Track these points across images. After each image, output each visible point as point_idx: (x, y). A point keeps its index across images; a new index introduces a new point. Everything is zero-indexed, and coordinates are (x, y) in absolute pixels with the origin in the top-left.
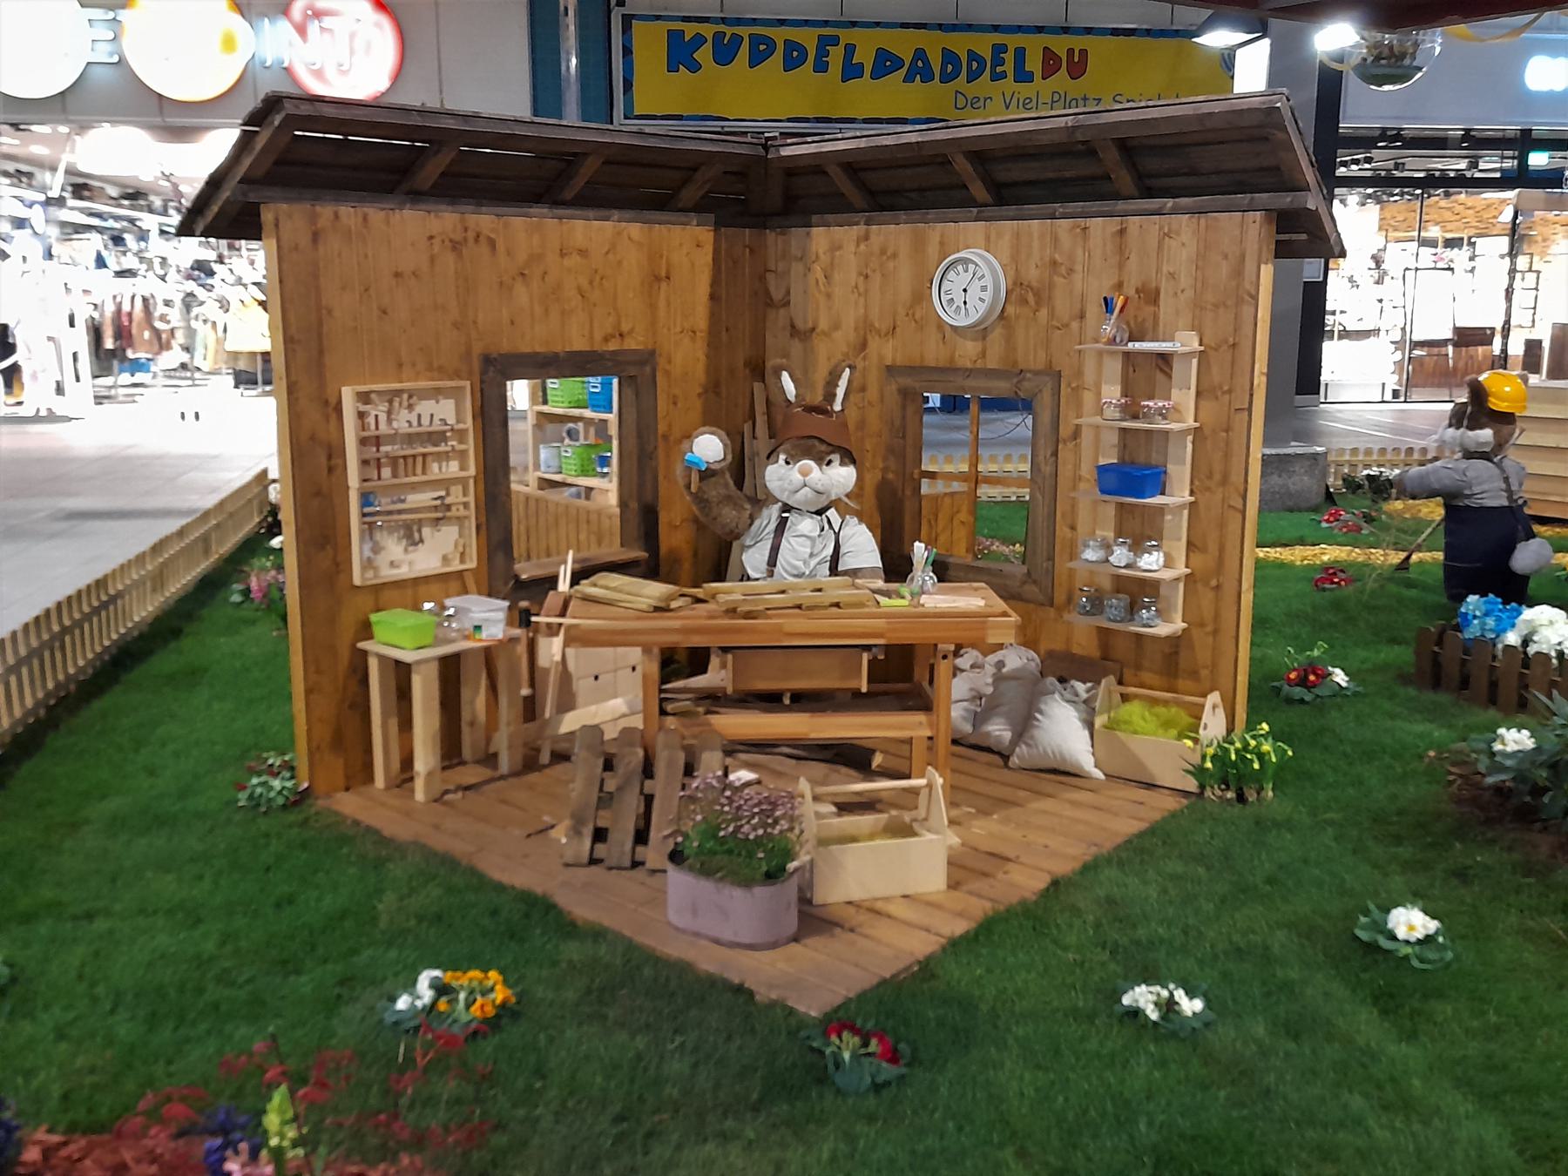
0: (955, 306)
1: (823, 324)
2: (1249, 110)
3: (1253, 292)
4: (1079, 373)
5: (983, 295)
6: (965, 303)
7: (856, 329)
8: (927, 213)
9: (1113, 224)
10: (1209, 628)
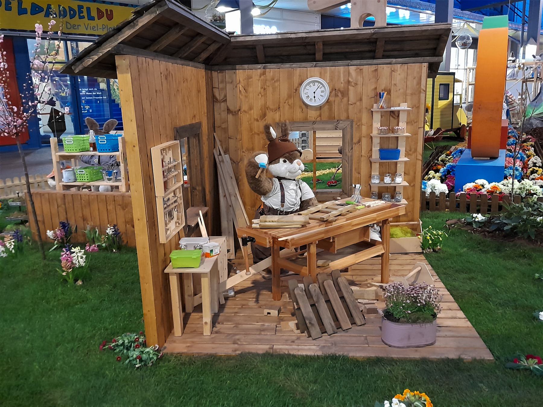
0: (310, 98)
1: (245, 107)
2: (441, 29)
3: (425, 89)
4: (360, 120)
5: (322, 94)
6: (314, 97)
7: (261, 109)
8: (293, 64)
9: (373, 68)
10: (411, 199)
